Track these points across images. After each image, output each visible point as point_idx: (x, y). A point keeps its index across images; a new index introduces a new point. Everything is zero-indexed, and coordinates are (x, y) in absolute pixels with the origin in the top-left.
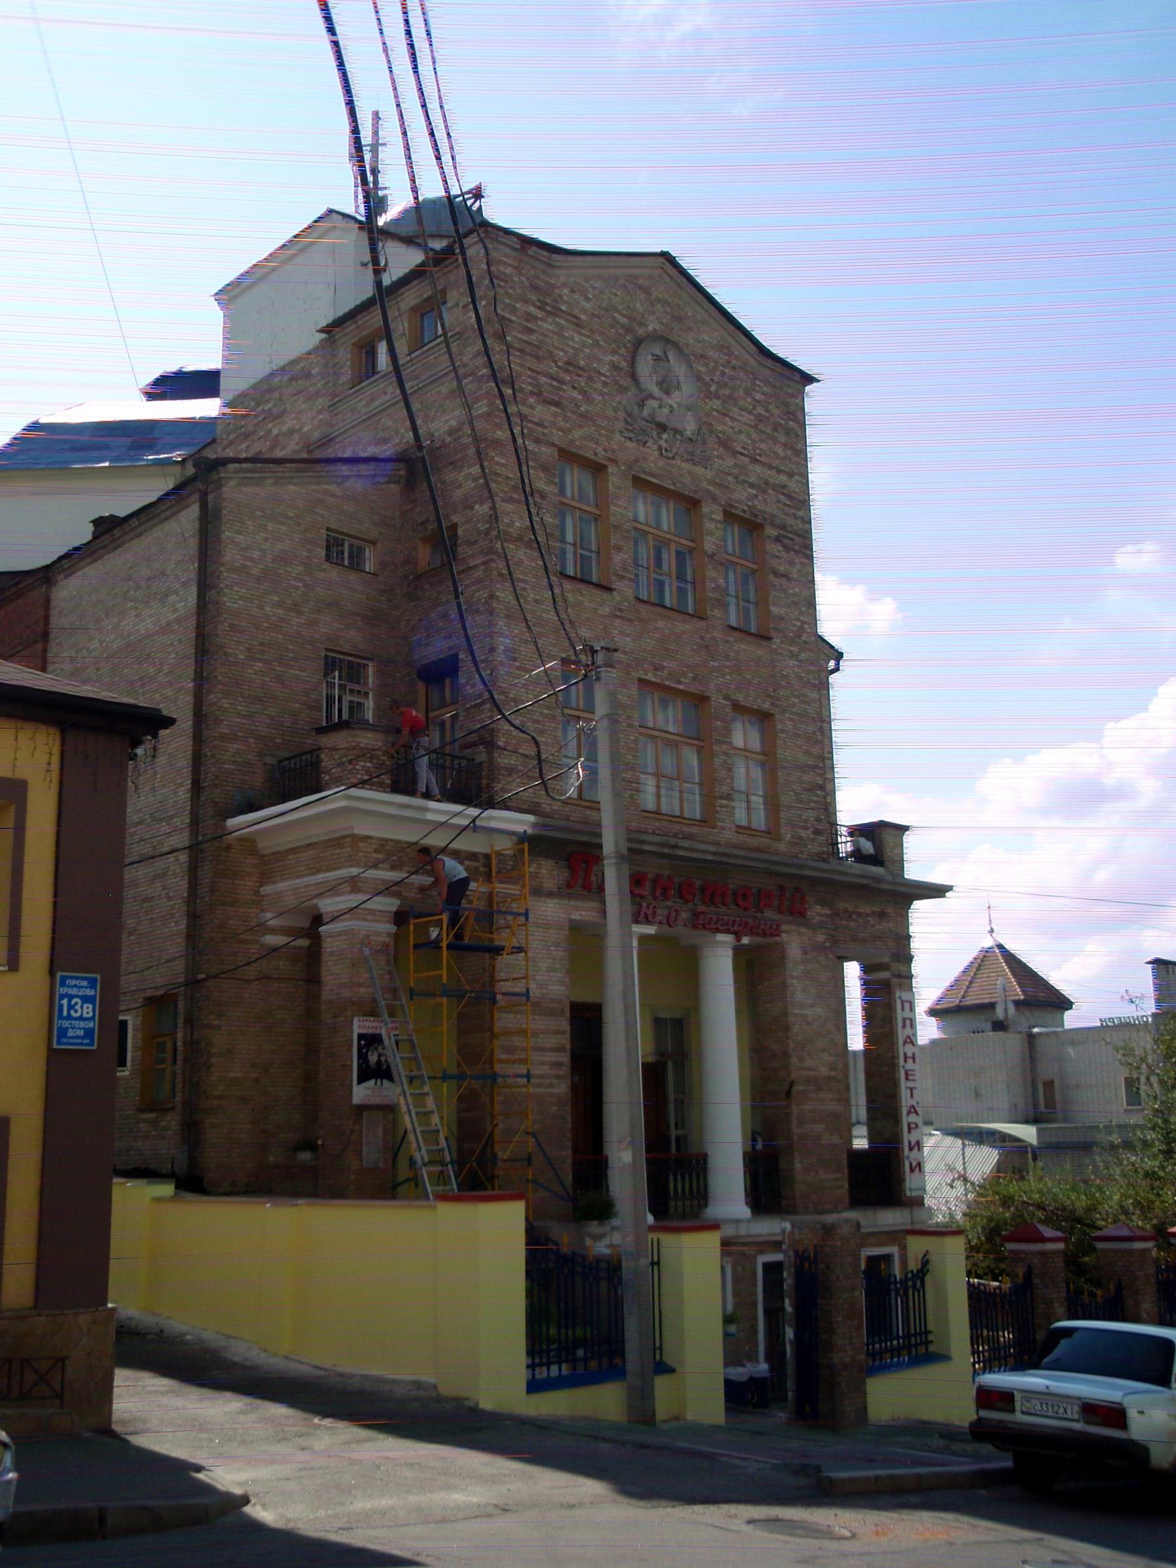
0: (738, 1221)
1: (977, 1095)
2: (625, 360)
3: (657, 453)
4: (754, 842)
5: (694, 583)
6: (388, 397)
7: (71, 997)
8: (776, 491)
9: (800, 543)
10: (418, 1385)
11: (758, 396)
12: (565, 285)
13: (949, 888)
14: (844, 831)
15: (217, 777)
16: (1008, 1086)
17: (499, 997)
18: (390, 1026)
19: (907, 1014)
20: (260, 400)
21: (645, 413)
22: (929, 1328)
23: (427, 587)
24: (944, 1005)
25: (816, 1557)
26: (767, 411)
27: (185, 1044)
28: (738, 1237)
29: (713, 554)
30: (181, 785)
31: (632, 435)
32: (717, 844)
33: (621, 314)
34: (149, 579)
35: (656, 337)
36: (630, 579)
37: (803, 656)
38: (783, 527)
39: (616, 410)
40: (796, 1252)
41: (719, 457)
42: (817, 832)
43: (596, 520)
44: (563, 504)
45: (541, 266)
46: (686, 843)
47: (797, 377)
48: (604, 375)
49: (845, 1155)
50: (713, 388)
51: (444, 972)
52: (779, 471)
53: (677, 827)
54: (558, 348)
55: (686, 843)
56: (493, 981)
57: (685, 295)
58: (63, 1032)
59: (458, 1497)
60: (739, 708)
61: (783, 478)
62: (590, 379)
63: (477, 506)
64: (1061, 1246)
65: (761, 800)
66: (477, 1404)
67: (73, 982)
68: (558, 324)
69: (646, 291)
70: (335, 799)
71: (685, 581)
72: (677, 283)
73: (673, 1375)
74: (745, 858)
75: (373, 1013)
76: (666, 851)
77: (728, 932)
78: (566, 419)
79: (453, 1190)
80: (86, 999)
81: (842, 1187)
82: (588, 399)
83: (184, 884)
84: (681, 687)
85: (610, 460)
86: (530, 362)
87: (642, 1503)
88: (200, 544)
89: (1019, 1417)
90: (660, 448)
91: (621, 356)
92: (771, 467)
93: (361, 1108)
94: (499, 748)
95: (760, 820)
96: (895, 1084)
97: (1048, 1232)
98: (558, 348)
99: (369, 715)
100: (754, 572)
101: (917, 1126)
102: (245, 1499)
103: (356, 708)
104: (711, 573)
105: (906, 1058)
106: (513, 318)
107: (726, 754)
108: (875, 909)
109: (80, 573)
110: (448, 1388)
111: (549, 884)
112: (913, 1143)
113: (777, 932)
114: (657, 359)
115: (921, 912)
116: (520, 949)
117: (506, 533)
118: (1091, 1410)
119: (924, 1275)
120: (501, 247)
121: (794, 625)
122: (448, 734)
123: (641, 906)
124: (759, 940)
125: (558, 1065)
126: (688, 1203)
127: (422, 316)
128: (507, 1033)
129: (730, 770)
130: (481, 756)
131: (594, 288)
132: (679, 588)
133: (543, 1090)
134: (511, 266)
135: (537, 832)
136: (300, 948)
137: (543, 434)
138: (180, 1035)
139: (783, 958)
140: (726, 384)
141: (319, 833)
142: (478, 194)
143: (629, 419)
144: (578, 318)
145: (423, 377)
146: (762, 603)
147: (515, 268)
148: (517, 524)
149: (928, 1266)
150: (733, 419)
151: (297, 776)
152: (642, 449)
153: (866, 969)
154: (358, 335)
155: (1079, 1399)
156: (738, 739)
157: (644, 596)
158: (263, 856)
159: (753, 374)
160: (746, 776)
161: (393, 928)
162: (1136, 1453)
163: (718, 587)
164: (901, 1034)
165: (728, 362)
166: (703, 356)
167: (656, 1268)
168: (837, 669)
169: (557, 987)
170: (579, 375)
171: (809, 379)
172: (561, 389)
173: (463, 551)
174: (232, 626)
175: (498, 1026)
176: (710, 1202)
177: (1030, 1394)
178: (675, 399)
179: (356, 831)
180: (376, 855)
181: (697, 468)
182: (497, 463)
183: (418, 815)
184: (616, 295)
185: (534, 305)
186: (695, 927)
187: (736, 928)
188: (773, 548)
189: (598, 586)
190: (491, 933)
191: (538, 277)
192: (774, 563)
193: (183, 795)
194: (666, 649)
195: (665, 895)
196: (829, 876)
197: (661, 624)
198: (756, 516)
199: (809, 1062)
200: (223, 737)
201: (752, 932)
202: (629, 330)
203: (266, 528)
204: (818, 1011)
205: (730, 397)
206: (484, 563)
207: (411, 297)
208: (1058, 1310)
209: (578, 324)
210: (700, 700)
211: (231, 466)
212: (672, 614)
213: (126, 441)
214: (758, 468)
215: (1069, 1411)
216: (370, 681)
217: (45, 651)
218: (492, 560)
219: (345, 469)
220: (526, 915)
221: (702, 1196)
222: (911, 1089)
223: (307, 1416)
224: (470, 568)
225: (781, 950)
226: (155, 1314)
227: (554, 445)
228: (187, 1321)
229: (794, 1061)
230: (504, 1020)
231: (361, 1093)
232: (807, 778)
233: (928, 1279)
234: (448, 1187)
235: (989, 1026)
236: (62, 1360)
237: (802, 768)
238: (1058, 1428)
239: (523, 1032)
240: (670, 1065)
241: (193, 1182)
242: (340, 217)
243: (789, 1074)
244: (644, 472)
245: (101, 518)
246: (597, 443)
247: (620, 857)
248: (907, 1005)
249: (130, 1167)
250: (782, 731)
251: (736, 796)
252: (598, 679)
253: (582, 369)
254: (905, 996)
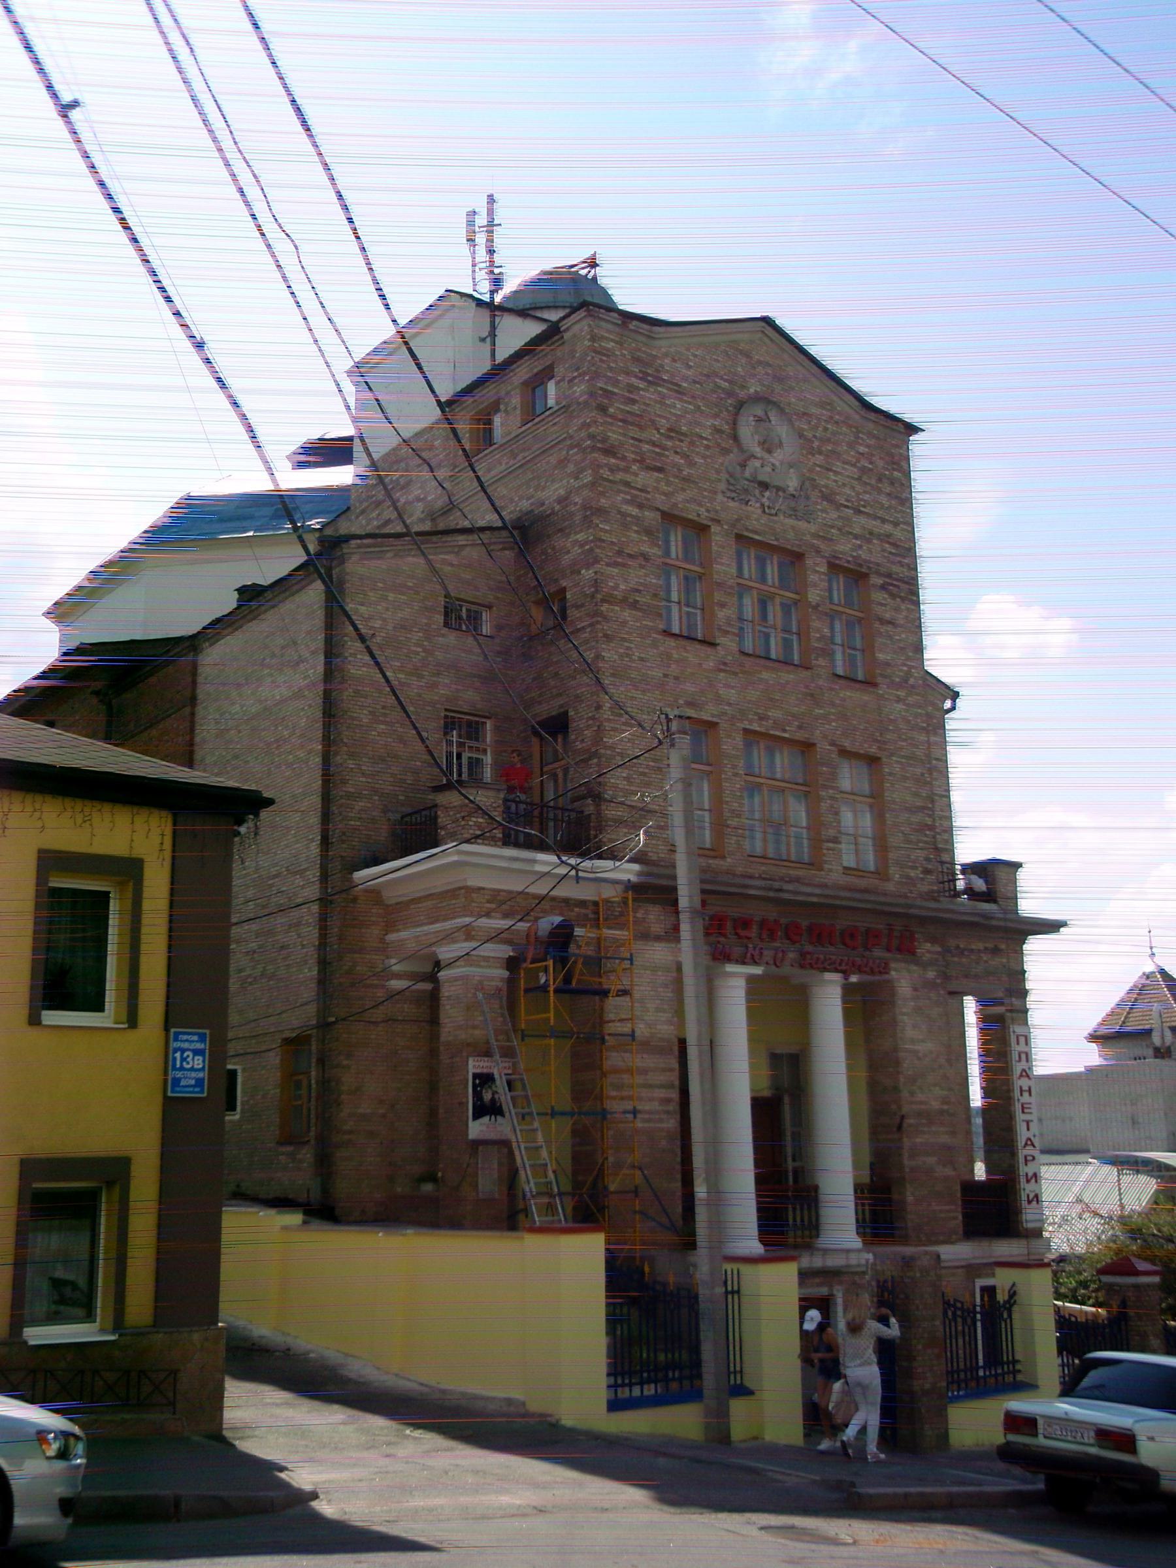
0: (848, 1251)
1: (1134, 1122)
2: (727, 423)
3: (759, 511)
4: (862, 883)
5: (799, 634)
6: (503, 467)
7: (183, 1051)
8: (882, 540)
9: (905, 588)
10: (509, 1401)
11: (862, 449)
12: (666, 355)
13: (1063, 924)
14: (959, 867)
15: (344, 833)
16: (1166, 1114)
17: (607, 1037)
18: (501, 1065)
19: (1022, 1047)
20: (382, 481)
21: (747, 474)
22: (1018, 1357)
23: (540, 648)
24: (1104, 1031)
25: (804, 1558)
26: (871, 463)
27: (317, 1083)
28: (848, 1266)
29: (818, 605)
30: (312, 840)
31: (733, 495)
32: (825, 886)
33: (722, 379)
34: (283, 648)
35: (757, 399)
36: (734, 634)
37: (910, 700)
38: (889, 576)
39: (718, 472)
40: (878, 1282)
41: (822, 511)
42: (927, 872)
43: (700, 578)
44: (666, 564)
45: (641, 338)
46: (790, 887)
47: (901, 428)
48: (706, 439)
49: (959, 1188)
50: (816, 444)
51: (552, 1015)
52: (884, 521)
53: (784, 871)
54: (659, 416)
55: (790, 887)
56: (602, 1022)
57: (785, 356)
58: (176, 1082)
59: (505, 1499)
60: (844, 753)
61: (888, 528)
62: (692, 443)
63: (583, 571)
64: (1156, 1279)
65: (870, 842)
66: (558, 1421)
67: (185, 1037)
68: (660, 393)
69: (748, 355)
70: (447, 854)
71: (789, 632)
73: (751, 1397)
74: (849, 899)
75: (488, 1054)
76: (771, 894)
77: (836, 971)
78: (668, 483)
79: (560, 1221)
80: (196, 1052)
81: (955, 1218)
82: (692, 464)
83: (315, 933)
84: (786, 735)
85: (713, 520)
86: (634, 432)
87: (672, 1510)
88: (326, 614)
89: (1041, 1440)
90: (763, 505)
91: (723, 419)
92: (876, 518)
93: (477, 1144)
94: (606, 800)
95: (870, 860)
96: (1011, 1117)
97: (1142, 1266)
98: (659, 416)
99: (488, 774)
100: (860, 620)
101: (1034, 1158)
102: (314, 1496)
103: (475, 764)
104: (816, 624)
105: (1021, 1091)
106: (616, 390)
107: (832, 798)
108: (987, 945)
109: (222, 642)
110: (534, 1406)
111: (657, 929)
112: (1030, 1175)
113: (885, 969)
114: (759, 420)
115: (1034, 946)
116: (625, 993)
117: (611, 595)
118: (1105, 1435)
119: (1011, 1306)
120: (603, 324)
121: (901, 671)
122: (560, 789)
123: (747, 947)
124: (867, 978)
125: (668, 1101)
126: (799, 1233)
127: (534, 389)
128: (617, 1071)
129: (837, 813)
130: (589, 807)
131: (696, 356)
132: (785, 639)
133: (652, 1125)
134: (612, 340)
135: (643, 879)
136: (424, 991)
137: (648, 500)
138: (313, 1073)
139: (893, 993)
140: (829, 440)
141: (440, 884)
142: (592, 263)
143: (732, 481)
144: (679, 386)
145: (534, 448)
146: (868, 649)
147: (616, 342)
148: (622, 587)
149: (1016, 1298)
150: (836, 473)
151: (417, 832)
152: (743, 507)
153: (984, 1003)
154: (470, 411)
155: (1095, 1424)
156: (846, 784)
157: (748, 646)
158: (388, 906)
159: (857, 428)
160: (855, 821)
161: (506, 974)
162: (1147, 1477)
163: (822, 638)
164: (1018, 1068)
165: (831, 418)
166: (804, 414)
167: (736, 1297)
168: (953, 708)
169: (666, 1027)
170: (682, 441)
171: (912, 429)
172: (663, 455)
173: (572, 613)
174: (357, 692)
175: (607, 1065)
176: (822, 1232)
177: (1051, 1420)
178: (778, 457)
179: (470, 883)
180: (488, 905)
181: (800, 523)
182: (602, 530)
183: (527, 867)
184: (718, 361)
185: (636, 377)
186: (802, 966)
187: (843, 967)
188: (879, 596)
189: (703, 642)
190: (600, 976)
191: (640, 350)
192: (878, 610)
193: (315, 849)
194: (771, 700)
195: (772, 936)
196: (934, 914)
197: (765, 675)
198: (861, 565)
199: (920, 1097)
200: (349, 796)
201: (860, 971)
202: (730, 394)
203: (389, 595)
204: (929, 1046)
205: (833, 452)
206: (591, 625)
207: (523, 372)
208: (1153, 1342)
209: (680, 392)
210: (806, 747)
211: (353, 542)
213: (268, 511)
214: (863, 520)
215: (1086, 1435)
216: (488, 740)
217: (193, 714)
218: (598, 622)
219: (461, 539)
220: (631, 960)
221: (813, 1227)
222: (1028, 1123)
223: (401, 1427)
224: (578, 630)
225: (889, 988)
226: (283, 1333)
227: (658, 509)
228: (312, 1341)
229: (905, 1094)
230: (613, 1059)
231: (477, 1129)
232: (916, 818)
233: (1015, 1308)
234: (556, 1218)
235: (1151, 1052)
236: (175, 1373)
237: (912, 810)
238: (1078, 1453)
239: (630, 1071)
240: (786, 1099)
241: (324, 1211)
242: (458, 296)
243: (900, 1107)
244: (747, 530)
245: (244, 586)
246: (700, 505)
247: (694, 912)
248: (1022, 1040)
249: (271, 1196)
250: (890, 774)
251: (844, 839)
252: (672, 745)
253: (685, 435)
254: (1019, 1030)
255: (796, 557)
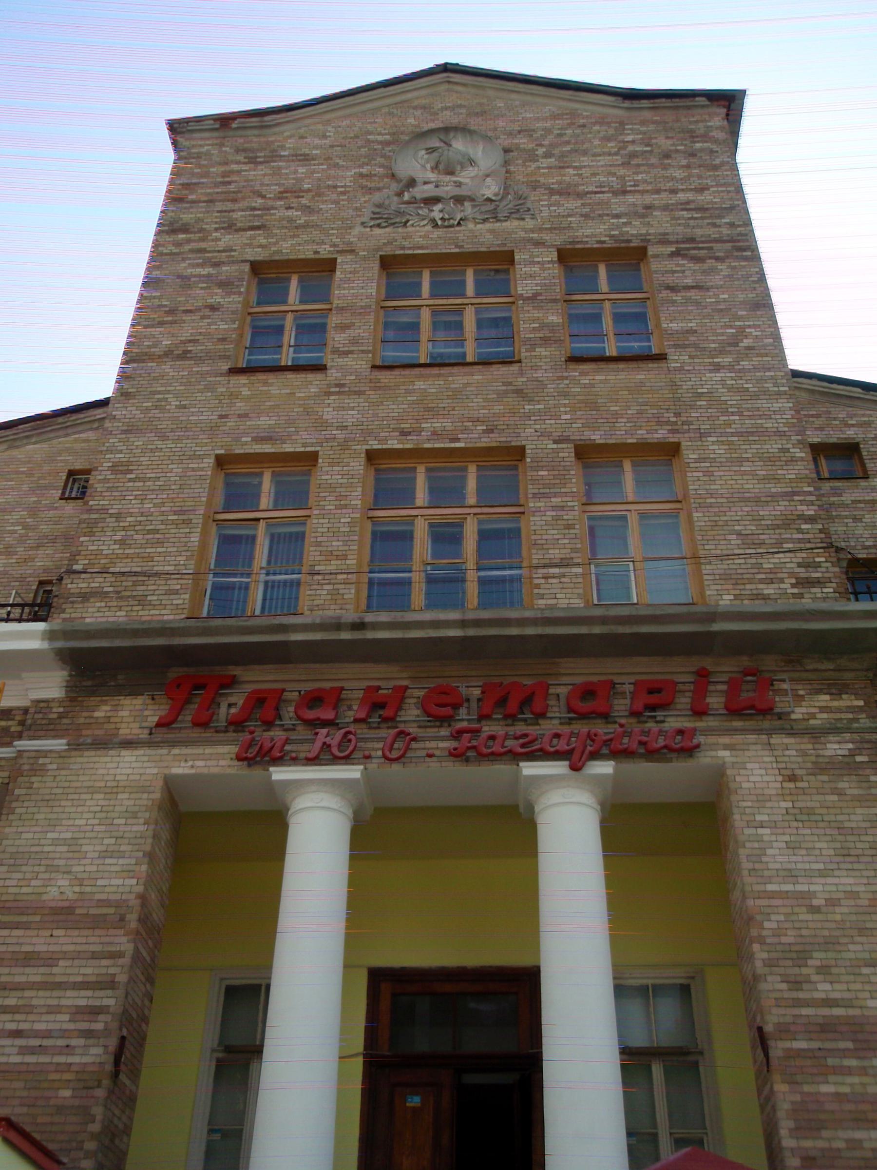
72: (474, 86)
198: (629, 241)
212: (428, 371)
255: (498, 263)
